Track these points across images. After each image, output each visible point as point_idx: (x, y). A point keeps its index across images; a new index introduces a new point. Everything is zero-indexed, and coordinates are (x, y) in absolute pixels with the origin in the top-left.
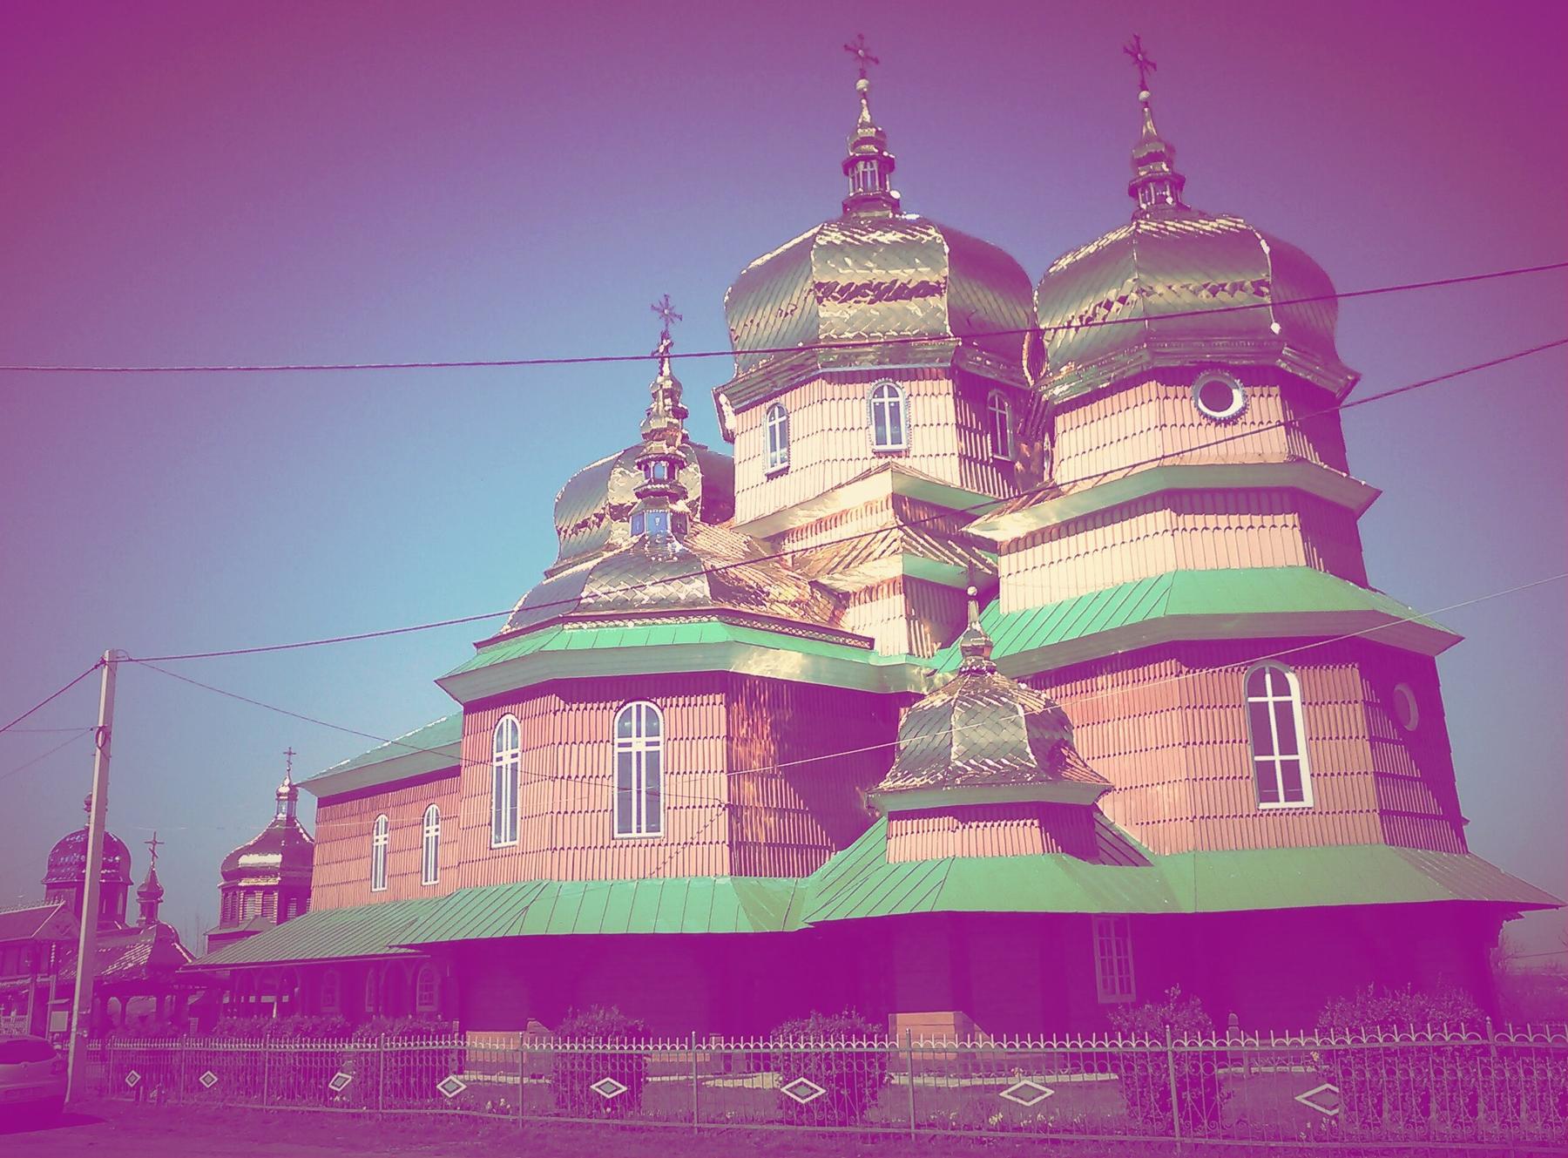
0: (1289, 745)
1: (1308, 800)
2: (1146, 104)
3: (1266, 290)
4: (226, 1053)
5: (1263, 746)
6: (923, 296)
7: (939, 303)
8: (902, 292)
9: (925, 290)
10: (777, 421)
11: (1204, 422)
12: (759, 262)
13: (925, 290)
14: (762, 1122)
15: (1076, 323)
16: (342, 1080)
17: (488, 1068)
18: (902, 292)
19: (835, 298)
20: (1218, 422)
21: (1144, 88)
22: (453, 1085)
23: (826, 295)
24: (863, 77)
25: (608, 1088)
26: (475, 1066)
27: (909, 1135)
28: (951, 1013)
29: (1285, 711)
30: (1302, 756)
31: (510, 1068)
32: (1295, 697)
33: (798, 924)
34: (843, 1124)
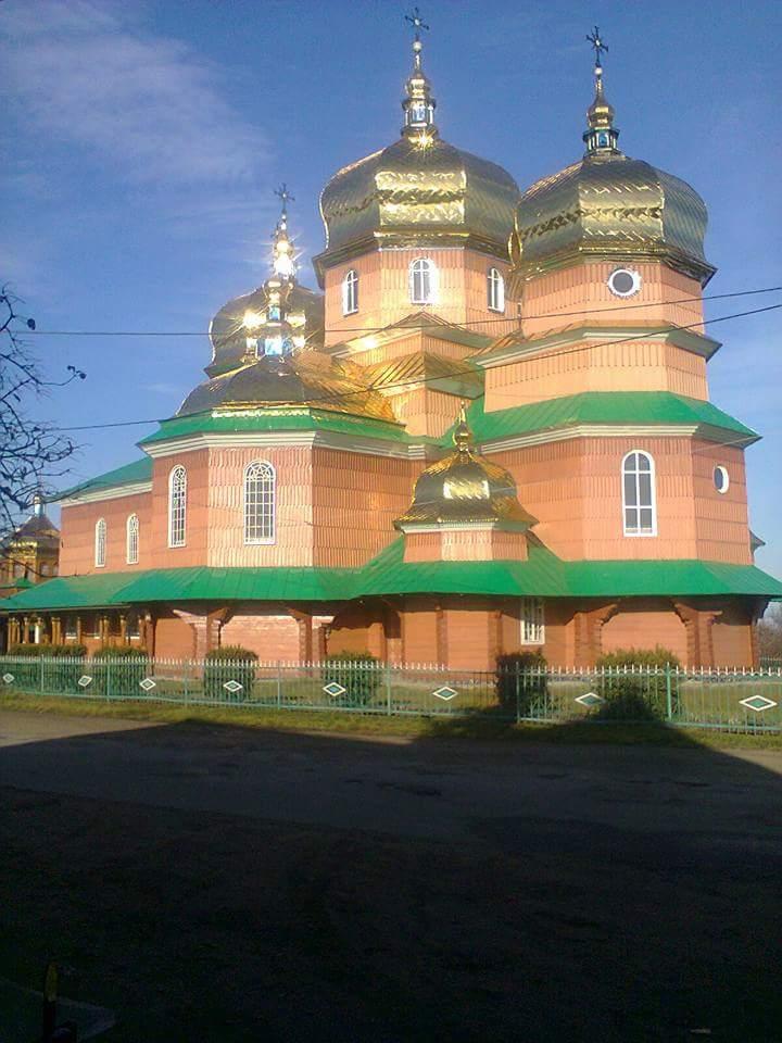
0: (646, 499)
1: (723, 490)
2: (599, 76)
3: (658, 213)
4: (18, 664)
5: (631, 500)
6: (449, 202)
7: (460, 206)
8: (434, 198)
9: (452, 197)
10: (353, 280)
11: (614, 298)
12: (343, 172)
13: (452, 197)
14: (90, 700)
15: (540, 230)
16: (86, 680)
17: (170, 673)
18: (434, 198)
19: (390, 201)
20: (622, 298)
21: (598, 66)
22: (148, 684)
23: (385, 198)
24: (417, 40)
25: (233, 686)
26: (161, 672)
27: (386, 714)
28: (485, 613)
29: (645, 480)
30: (653, 507)
31: (178, 673)
32: (652, 472)
33: (354, 595)
34: (354, 706)
